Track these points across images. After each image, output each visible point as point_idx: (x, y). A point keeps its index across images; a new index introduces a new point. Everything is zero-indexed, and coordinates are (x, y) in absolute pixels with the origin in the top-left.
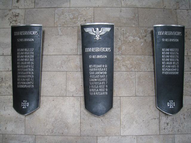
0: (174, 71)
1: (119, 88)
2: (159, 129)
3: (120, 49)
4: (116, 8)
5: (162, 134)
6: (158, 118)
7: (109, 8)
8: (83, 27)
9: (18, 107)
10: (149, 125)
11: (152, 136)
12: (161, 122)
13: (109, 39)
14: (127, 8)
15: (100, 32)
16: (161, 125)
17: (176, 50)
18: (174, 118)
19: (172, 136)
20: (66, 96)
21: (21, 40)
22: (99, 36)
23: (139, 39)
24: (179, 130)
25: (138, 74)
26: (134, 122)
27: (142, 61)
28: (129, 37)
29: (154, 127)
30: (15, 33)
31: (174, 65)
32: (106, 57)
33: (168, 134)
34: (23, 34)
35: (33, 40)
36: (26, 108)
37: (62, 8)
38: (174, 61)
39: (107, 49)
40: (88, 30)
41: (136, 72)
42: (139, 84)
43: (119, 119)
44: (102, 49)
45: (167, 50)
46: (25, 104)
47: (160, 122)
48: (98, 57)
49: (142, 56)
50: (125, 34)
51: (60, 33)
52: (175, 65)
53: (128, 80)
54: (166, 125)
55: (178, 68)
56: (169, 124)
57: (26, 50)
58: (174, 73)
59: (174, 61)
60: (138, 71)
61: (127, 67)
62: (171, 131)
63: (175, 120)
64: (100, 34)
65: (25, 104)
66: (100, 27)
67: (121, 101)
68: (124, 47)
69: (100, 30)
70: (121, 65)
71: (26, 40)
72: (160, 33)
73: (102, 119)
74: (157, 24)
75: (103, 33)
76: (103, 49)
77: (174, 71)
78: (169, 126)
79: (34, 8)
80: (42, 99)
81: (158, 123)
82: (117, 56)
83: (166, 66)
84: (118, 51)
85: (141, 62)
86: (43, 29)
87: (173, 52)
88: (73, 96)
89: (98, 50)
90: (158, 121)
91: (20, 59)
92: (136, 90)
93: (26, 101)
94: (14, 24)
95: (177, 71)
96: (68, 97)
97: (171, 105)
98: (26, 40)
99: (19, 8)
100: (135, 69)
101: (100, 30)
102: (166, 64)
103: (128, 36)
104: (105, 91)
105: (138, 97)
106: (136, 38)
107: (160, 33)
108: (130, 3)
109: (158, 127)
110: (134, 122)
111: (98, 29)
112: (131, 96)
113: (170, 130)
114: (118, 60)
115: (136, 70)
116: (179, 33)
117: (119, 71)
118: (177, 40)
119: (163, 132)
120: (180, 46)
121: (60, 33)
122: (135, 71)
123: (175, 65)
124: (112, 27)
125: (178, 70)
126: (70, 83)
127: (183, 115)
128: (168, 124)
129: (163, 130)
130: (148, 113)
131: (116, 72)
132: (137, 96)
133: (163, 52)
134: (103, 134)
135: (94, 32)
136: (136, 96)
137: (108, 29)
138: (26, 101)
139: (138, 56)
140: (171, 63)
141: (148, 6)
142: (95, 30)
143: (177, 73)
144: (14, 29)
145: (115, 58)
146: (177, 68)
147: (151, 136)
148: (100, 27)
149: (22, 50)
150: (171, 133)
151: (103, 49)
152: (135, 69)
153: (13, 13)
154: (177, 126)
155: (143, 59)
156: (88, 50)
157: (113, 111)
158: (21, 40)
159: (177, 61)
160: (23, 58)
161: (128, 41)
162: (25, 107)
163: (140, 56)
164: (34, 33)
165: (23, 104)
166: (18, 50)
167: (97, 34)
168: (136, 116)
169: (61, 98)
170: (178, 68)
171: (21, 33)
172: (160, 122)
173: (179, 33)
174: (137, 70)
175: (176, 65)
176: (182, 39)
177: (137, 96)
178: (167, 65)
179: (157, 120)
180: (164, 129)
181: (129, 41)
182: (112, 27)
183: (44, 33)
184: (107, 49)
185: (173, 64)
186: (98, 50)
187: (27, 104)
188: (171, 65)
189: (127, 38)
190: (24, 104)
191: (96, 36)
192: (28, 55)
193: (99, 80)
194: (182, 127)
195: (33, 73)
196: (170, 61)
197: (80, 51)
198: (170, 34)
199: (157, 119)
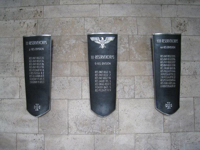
8: (89, 36)
9: (30, 109)
13: (113, 48)
15: (105, 41)
21: (32, 49)
22: (104, 45)
32: (110, 64)
35: (43, 49)
36: (38, 110)
39: (111, 57)
40: (92, 39)
44: (106, 56)
45: (165, 56)
46: (37, 107)
48: (103, 63)
64: (105, 43)
66: (105, 36)
69: (105, 39)
71: (37, 49)
72: (159, 41)
74: (46, 34)
75: (108, 42)
76: (106, 57)
86: (52, 38)
87: (39, 60)
89: (102, 57)
93: (172, 106)
94: (25, 35)
97: (168, 106)
98: (37, 49)
101: (105, 39)
107: (159, 41)
111: (103, 38)
116: (175, 41)
118: (174, 47)
120: (176, 52)
124: (116, 36)
133: (30, 60)
135: (100, 41)
137: (111, 39)
138: (172, 106)
140: (168, 68)
142: (101, 39)
144: (25, 39)
148: (105, 36)
149: (34, 58)
151: (106, 57)
156: (92, 57)
157: (115, 112)
166: (30, 58)
167: (102, 43)
171: (30, 43)
173: (175, 41)
176: (178, 45)
182: (116, 36)
183: (52, 41)
184: (111, 57)
186: (102, 57)
191: (101, 45)
192: (40, 62)
196: (167, 66)
197: (87, 59)
198: (167, 42)
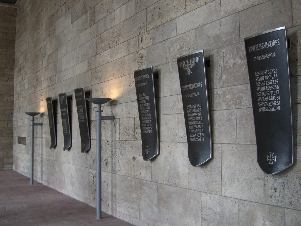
0: (274, 106)
1: (220, 132)
2: (264, 195)
3: (220, 79)
4: (216, 22)
5: (268, 204)
6: (263, 179)
7: (209, 24)
10: (252, 186)
11: (256, 204)
12: (267, 185)
14: (227, 18)
16: (266, 189)
17: (273, 72)
18: (286, 182)
19: (281, 210)
20: (177, 142)
21: (259, 58)
23: (240, 61)
24: (292, 203)
25: (239, 113)
26: (236, 180)
27: (244, 93)
28: (229, 60)
29: (258, 192)
30: (249, 49)
31: (272, 95)
33: (276, 206)
34: (259, 48)
35: (274, 55)
37: (171, 39)
38: (271, 90)
41: (237, 110)
42: (240, 127)
43: (220, 174)
47: (265, 185)
49: (244, 85)
50: (225, 58)
51: (171, 70)
52: (274, 95)
53: (228, 122)
54: (273, 191)
55: (279, 100)
56: (277, 191)
57: (266, 72)
58: (274, 109)
59: (271, 90)
60: (239, 109)
61: (227, 103)
62: (280, 201)
63: (286, 185)
65: (271, 158)
67: (222, 150)
68: (224, 77)
70: (222, 102)
71: (264, 57)
73: (205, 171)
77: (274, 106)
78: (277, 194)
79: (152, 45)
80: (161, 144)
81: (263, 186)
82: (218, 89)
83: (262, 98)
84: (219, 83)
85: (242, 95)
87: (268, 75)
88: (182, 142)
90: (263, 183)
91: (260, 88)
92: (238, 134)
93: (273, 153)
95: (278, 106)
96: (178, 143)
98: (264, 57)
99: (143, 48)
100: (235, 106)
102: (262, 95)
103: (228, 59)
104: (202, 137)
105: (239, 145)
106: (237, 60)
108: (230, 8)
109: (263, 192)
110: (236, 180)
112: (232, 144)
113: (280, 199)
114: (219, 95)
115: (237, 107)
117: (219, 110)
119: (269, 201)
121: (171, 70)
122: (236, 109)
123: (274, 95)
125: (279, 103)
126: (180, 127)
127: (298, 179)
128: (275, 189)
129: (270, 198)
130: (250, 168)
131: (217, 111)
132: (238, 144)
134: (206, 190)
135: (186, 66)
136: (237, 144)
138: (273, 153)
139: (239, 86)
141: (251, 3)
143: (278, 108)
145: (216, 93)
146: (277, 101)
147: (254, 203)
149: (262, 73)
150: (280, 204)
152: (235, 106)
153: (139, 54)
154: (289, 195)
155: (245, 90)
158: (259, 58)
159: (277, 89)
160: (264, 86)
161: (229, 67)
162: (271, 162)
163: (241, 86)
164: (274, 43)
165: (269, 158)
168: (238, 172)
169: (174, 143)
170: (279, 100)
172: (265, 185)
174: (238, 107)
175: (276, 96)
177: (238, 144)
178: (263, 96)
179: (261, 182)
180: (271, 196)
181: (229, 66)
185: (270, 94)
187: (274, 158)
188: (269, 96)
189: (227, 62)
190: (270, 158)
193: (196, 123)
194: (296, 198)
195: (150, 117)
199: (261, 180)
